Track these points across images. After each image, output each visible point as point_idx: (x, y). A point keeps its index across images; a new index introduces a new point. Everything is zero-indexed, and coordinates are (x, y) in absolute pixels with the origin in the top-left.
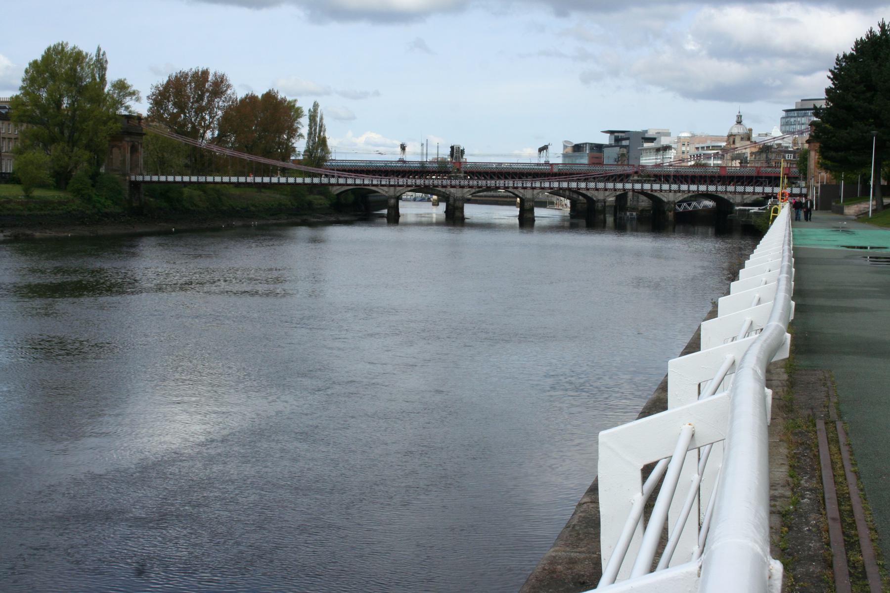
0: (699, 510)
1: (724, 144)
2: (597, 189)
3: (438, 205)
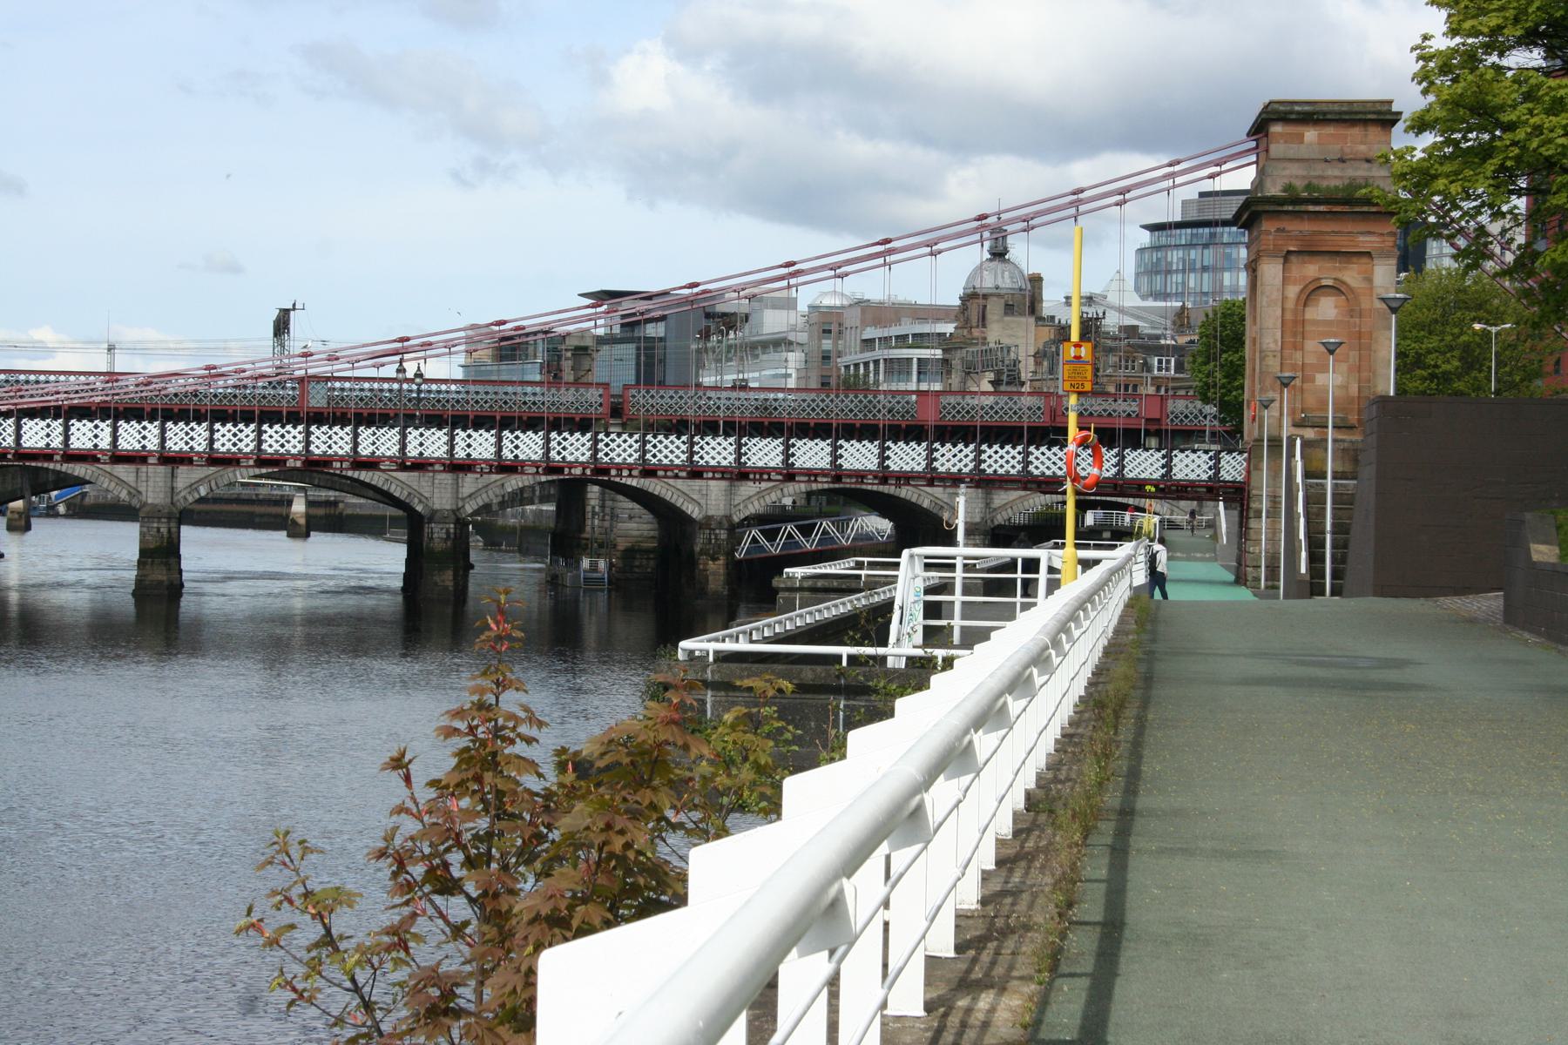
0: (995, 751)
1: (948, 328)
2: (696, 473)
3: (28, 528)
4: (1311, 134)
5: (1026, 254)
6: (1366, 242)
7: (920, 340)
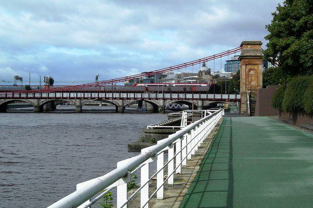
4: (249, 46)
5: (209, 64)
6: (258, 62)
7: (192, 79)
